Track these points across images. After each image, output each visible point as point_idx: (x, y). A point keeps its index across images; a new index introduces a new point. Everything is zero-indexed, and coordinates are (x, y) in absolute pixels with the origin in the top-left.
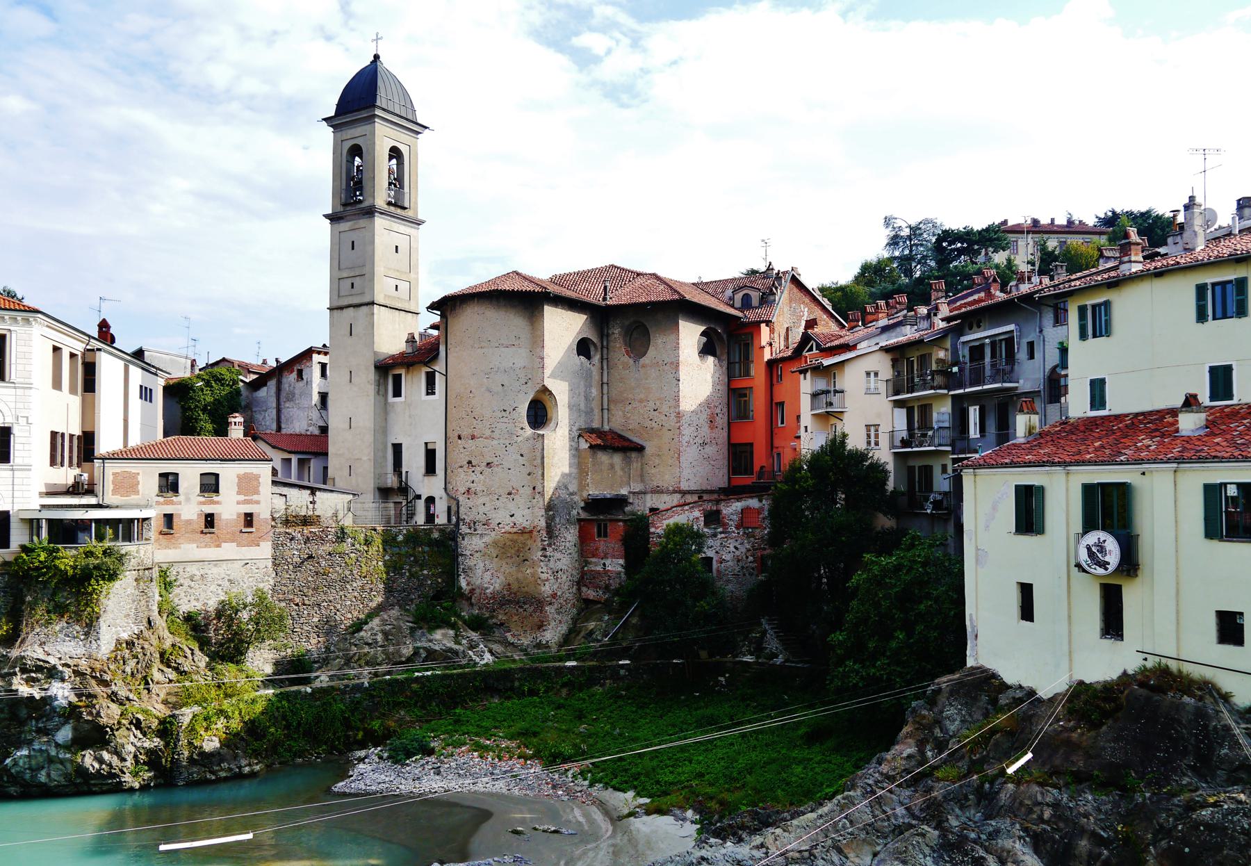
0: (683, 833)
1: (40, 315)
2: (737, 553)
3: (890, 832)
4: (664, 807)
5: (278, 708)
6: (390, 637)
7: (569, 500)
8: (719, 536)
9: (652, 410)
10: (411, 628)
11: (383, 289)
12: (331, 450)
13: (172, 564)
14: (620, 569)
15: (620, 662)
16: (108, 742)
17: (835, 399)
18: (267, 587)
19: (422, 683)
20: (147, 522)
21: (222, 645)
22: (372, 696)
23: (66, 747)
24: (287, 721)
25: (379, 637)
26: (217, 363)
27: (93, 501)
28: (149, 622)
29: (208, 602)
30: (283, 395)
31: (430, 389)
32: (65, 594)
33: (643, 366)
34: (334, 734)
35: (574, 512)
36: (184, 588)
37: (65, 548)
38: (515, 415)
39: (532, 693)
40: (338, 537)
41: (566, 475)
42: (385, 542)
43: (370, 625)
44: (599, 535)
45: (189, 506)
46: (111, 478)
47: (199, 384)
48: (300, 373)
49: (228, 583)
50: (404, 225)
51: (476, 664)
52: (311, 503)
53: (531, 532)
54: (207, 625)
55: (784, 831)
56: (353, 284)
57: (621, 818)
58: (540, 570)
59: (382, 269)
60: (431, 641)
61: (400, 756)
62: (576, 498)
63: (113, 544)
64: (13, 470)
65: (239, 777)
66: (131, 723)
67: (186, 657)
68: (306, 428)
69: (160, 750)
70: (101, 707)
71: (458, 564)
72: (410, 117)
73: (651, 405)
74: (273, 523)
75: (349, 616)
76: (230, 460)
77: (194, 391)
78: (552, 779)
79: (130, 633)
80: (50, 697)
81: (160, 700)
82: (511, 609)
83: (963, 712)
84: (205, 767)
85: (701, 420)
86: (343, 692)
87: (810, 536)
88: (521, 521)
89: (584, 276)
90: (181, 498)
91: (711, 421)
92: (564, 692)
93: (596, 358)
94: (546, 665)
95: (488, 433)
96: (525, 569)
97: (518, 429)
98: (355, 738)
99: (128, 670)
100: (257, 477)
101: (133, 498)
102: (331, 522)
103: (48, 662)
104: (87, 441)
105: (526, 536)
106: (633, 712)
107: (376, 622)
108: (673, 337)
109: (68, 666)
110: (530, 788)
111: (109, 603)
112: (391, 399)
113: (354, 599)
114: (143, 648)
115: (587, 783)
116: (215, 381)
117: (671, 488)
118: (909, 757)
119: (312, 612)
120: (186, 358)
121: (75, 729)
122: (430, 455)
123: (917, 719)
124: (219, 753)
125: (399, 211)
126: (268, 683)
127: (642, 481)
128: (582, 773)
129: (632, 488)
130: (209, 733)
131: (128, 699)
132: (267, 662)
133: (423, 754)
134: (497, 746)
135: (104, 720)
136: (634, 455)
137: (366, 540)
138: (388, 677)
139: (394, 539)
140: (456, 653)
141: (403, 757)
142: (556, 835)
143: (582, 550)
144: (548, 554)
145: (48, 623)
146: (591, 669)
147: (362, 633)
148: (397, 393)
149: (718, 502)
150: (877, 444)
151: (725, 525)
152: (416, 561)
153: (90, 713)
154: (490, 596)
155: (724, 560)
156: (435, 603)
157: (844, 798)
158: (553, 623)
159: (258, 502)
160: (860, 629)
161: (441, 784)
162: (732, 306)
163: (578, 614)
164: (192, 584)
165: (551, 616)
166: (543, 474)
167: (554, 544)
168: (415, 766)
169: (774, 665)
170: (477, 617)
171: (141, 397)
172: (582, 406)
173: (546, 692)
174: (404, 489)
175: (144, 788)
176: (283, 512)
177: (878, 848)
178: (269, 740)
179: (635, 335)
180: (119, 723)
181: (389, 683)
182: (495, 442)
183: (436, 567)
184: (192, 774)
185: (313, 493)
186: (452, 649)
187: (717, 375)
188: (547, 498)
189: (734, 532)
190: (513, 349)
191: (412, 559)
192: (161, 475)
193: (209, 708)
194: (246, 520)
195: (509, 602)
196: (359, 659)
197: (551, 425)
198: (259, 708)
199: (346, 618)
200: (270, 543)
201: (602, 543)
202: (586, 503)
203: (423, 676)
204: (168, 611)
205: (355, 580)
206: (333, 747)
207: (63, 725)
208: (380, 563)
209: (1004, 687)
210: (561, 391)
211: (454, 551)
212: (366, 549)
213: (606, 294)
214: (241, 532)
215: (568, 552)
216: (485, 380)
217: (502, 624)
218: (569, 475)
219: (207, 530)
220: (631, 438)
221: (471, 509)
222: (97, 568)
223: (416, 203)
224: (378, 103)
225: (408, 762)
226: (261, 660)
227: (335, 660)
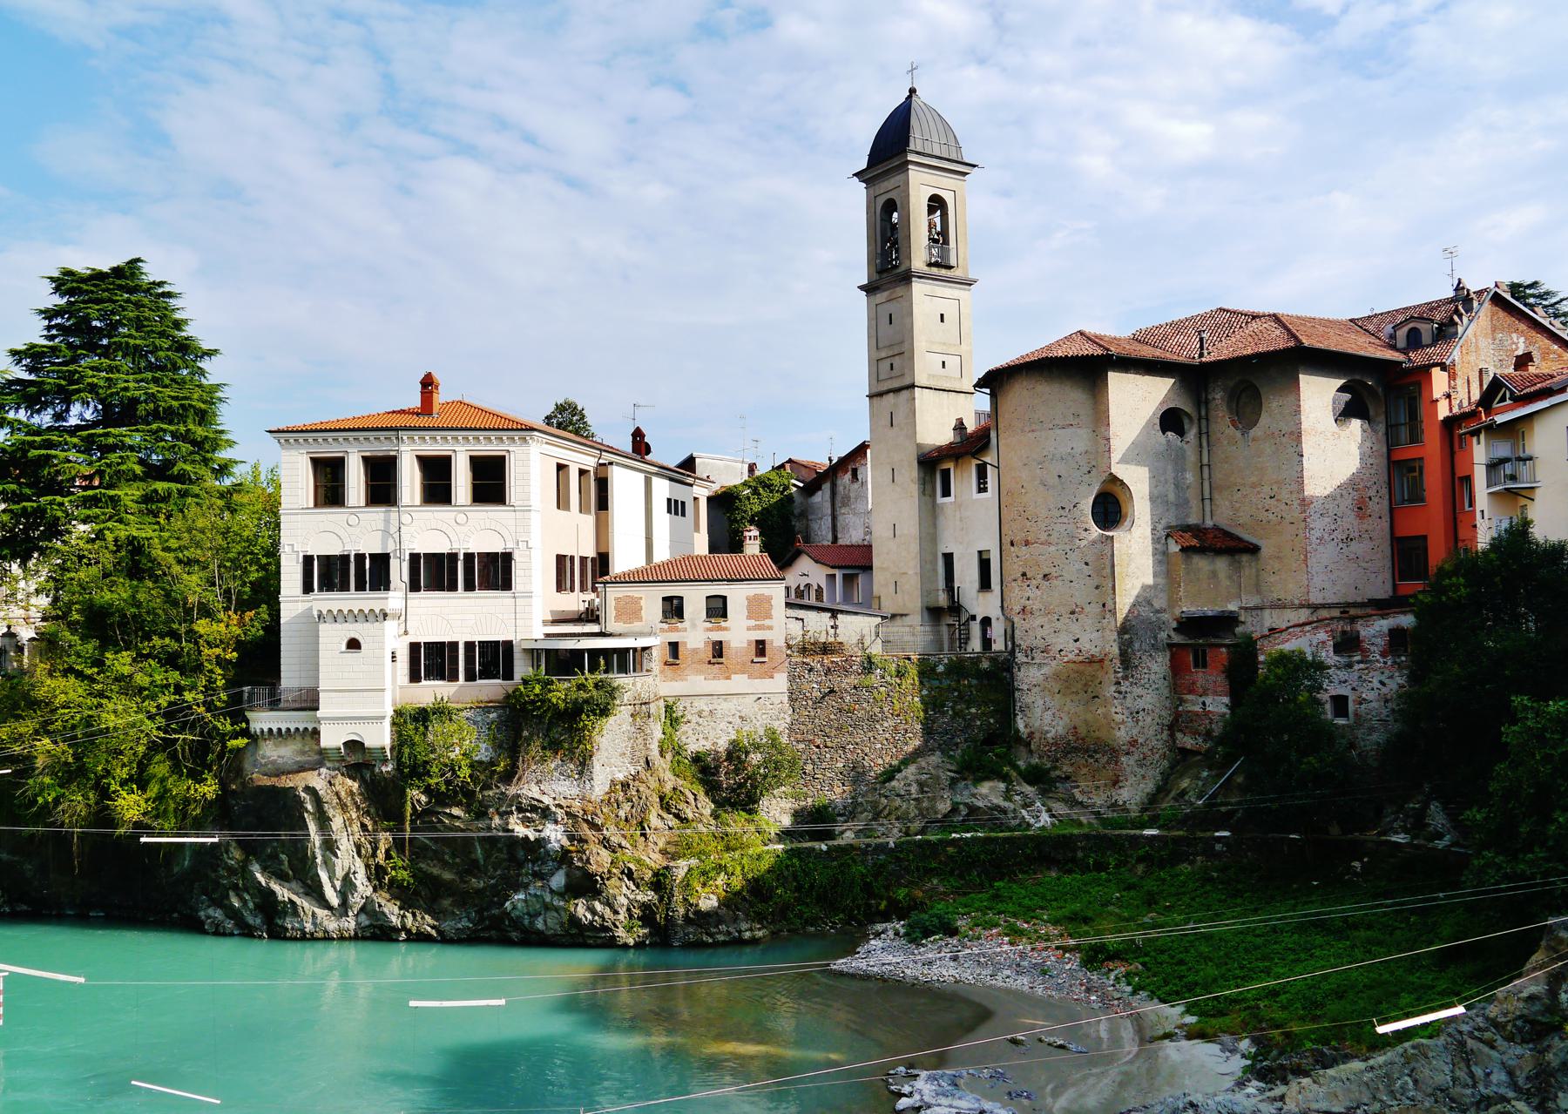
0: (1224, 1069)
1: (536, 433)
2: (1384, 690)
3: (1473, 1104)
4: (1210, 1031)
5: (787, 866)
6: (925, 789)
8: (1356, 667)
9: (1268, 497)
10: (952, 778)
11: (925, 368)
12: (876, 563)
13: (678, 697)
14: (1225, 710)
15: (1217, 834)
16: (599, 892)
17: (1524, 470)
18: (781, 726)
19: (960, 847)
20: (647, 651)
21: (733, 790)
22: (898, 859)
23: (561, 895)
24: (798, 882)
25: (914, 789)
27: (595, 628)
28: (647, 762)
29: (718, 741)
30: (839, 498)
32: (560, 729)
33: (1254, 440)
34: (853, 901)
35: (1163, 635)
36: (693, 725)
37: (559, 680)
38: (1076, 512)
39: (1100, 867)
40: (864, 668)
41: (1149, 586)
42: (921, 674)
43: (904, 773)
44: (1196, 666)
45: (695, 632)
46: (613, 603)
47: (745, 492)
48: (855, 473)
49: (739, 721)
50: (950, 287)
51: (1029, 825)
52: (832, 627)
53: (1101, 661)
54: (717, 768)
55: (1315, 1082)
56: (892, 365)
57: (1153, 1040)
58: (1113, 710)
59: (924, 344)
60: (974, 795)
61: (917, 935)
62: (1165, 617)
63: (606, 676)
64: (514, 597)
65: (738, 942)
66: (623, 873)
67: (687, 802)
68: (862, 537)
69: (654, 904)
70: (591, 853)
71: (1014, 701)
72: (960, 160)
73: (1266, 489)
74: (789, 652)
75: (880, 761)
76: (737, 580)
77: (740, 500)
78: (1090, 980)
79: (626, 774)
80: (544, 839)
81: (657, 850)
82: (1080, 760)
84: (701, 928)
85: (1342, 508)
86: (865, 852)
87: (1457, 669)
88: (1088, 646)
89: (1178, 327)
90: (686, 624)
91: (1360, 508)
92: (1140, 868)
93: (1192, 434)
94: (1117, 832)
95: (1043, 537)
96: (1095, 708)
97: (1080, 531)
98: (877, 907)
99: (622, 814)
100: (769, 599)
101: (636, 626)
102: (856, 649)
103: (541, 802)
104: (602, 562)
105: (1096, 666)
106: (1220, 901)
107: (912, 769)
108: (1291, 398)
109: (561, 807)
110: (1059, 988)
111: (604, 739)
112: (940, 500)
113: (885, 742)
114: (638, 791)
115: (1129, 989)
116: (763, 488)
117: (1297, 602)
118: (1532, 998)
119: (836, 756)
120: (743, 462)
121: (568, 875)
122: (984, 565)
123: (1553, 944)
124: (716, 913)
125: (943, 272)
126: (785, 835)
127: (1258, 592)
128: (1127, 975)
129: (1244, 601)
130: (706, 890)
131: (620, 846)
132: (783, 811)
133: (945, 934)
134: (1036, 931)
135: (593, 868)
136: (1245, 558)
137: (899, 672)
139: (933, 669)
140: (1004, 811)
141: (920, 936)
142: (1061, 1051)
143: (1175, 684)
144: (1123, 689)
145: (543, 760)
146: (1176, 840)
147: (894, 783)
148: (946, 493)
149: (1353, 619)
151: (1364, 651)
152: (961, 697)
153: (580, 859)
154: (1051, 741)
155: (1364, 699)
156: (987, 748)
157: (1413, 1047)
158: (1132, 779)
159: (770, 628)
160: (1510, 806)
161: (952, 972)
162: (1393, 347)
163: (1172, 768)
164: (701, 721)
165: (1128, 769)
166: (1114, 586)
167: (1132, 676)
168: (929, 950)
169: (1435, 849)
170: (1036, 767)
171: (669, 511)
172: (1172, 497)
173: (1117, 866)
174: (955, 608)
175: (639, 946)
176: (800, 638)
178: (776, 903)
180: (609, 872)
181: (920, 844)
182: (1052, 548)
183: (986, 705)
184: (687, 934)
186: (999, 807)
187: (1368, 444)
188: (1120, 617)
189: (1377, 661)
190: (1069, 431)
191: (956, 694)
192: (664, 599)
193: (707, 862)
194: (757, 648)
195: (1076, 750)
196: (889, 814)
197: (1126, 524)
198: (765, 865)
199: (877, 763)
200: (786, 674)
201: (1201, 675)
202: (1178, 622)
203: (961, 839)
204: (671, 747)
205: (885, 719)
206: (852, 917)
207: (557, 870)
208: (916, 699)
210: (1138, 481)
211: (1009, 684)
212: (899, 682)
213: (1202, 347)
214: (752, 662)
216: (1038, 471)
217: (1067, 778)
218: (1155, 587)
219: (713, 660)
221: (1032, 632)
222: (586, 701)
224: (912, 147)
225: (924, 941)
226: (777, 811)
227: (862, 813)
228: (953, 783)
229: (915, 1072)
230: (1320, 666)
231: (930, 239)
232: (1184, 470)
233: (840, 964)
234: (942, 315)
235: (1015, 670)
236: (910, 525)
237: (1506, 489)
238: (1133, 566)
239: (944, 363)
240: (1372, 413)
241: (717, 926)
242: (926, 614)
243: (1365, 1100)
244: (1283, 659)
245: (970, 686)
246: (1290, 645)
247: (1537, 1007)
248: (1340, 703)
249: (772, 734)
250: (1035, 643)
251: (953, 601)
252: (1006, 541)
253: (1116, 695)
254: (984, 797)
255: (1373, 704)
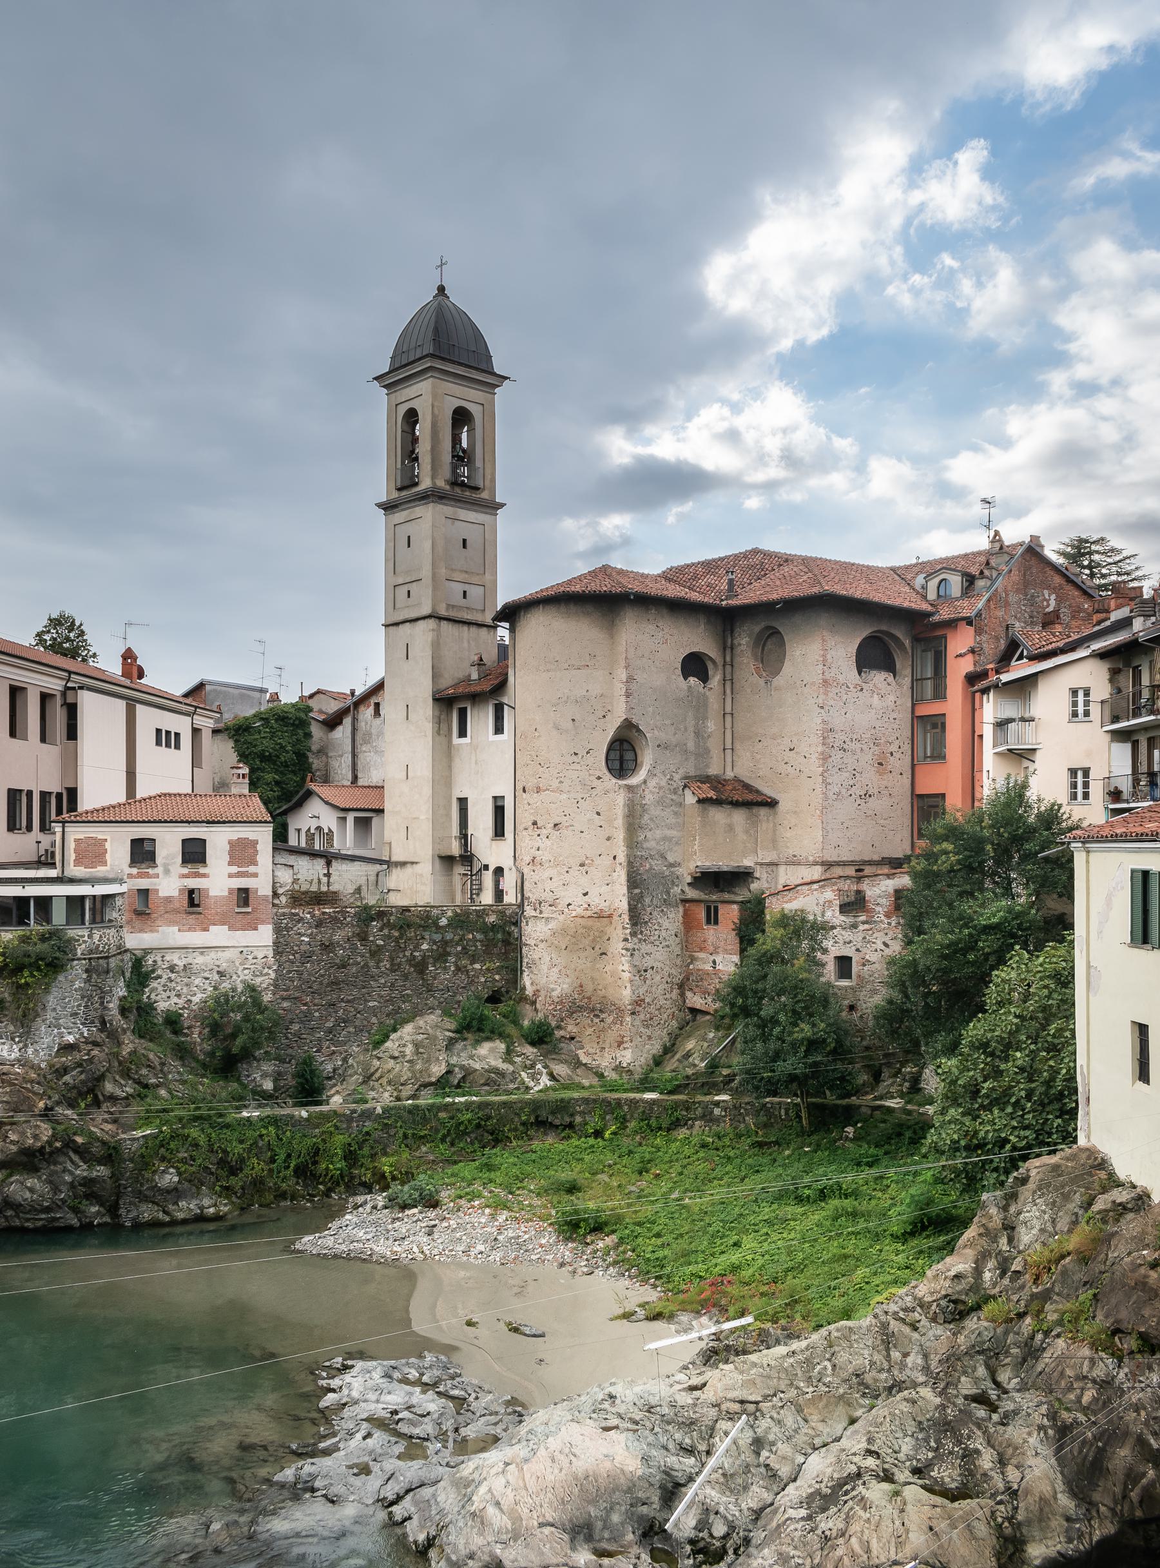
2: (888, 952)
6: (421, 1050)
7: (667, 873)
8: (861, 927)
10: (451, 1039)
13: (147, 952)
25: (409, 1050)
26: (311, 696)
27: (53, 873)
29: (193, 999)
31: (499, 729)
35: (676, 890)
36: (163, 981)
44: (708, 922)
48: (377, 705)
49: (216, 977)
53: (610, 916)
59: (444, 570)
72: (483, 366)
73: (786, 741)
82: (585, 1019)
83: (1046, 1217)
86: (349, 1119)
88: (597, 901)
89: (710, 566)
90: (159, 870)
94: (617, 1095)
95: (555, 784)
112: (456, 741)
118: (958, 1277)
122: (499, 811)
136: (763, 812)
138: (410, 1102)
146: (676, 1106)
148: (463, 733)
150: (1086, 796)
154: (557, 1000)
159: (255, 875)
164: (173, 976)
167: (641, 933)
174: (467, 858)
177: (859, 1413)
179: (769, 645)
181: (412, 1111)
182: (564, 796)
185: (329, 864)
200: (270, 927)
201: (712, 932)
209: (1113, 1182)
215: (664, 944)
220: (760, 788)
223: (493, 480)
227: (351, 1076)
228: (450, 1044)
229: (350, 1363)
230: (827, 927)
231: (453, 457)
232: (705, 718)
233: (307, 1242)
234: (464, 541)
235: (524, 924)
236: (423, 768)
237: (1009, 750)
238: (646, 817)
239: (465, 592)
240: (898, 666)
241: (176, 1203)
242: (437, 860)
243: (783, 1388)
244: (784, 921)
245: (474, 939)
246: (792, 905)
247: (963, 1285)
248: (844, 964)
249: (251, 989)
250: (544, 896)
251: (466, 851)
252: (519, 787)
253: (624, 952)
254: (482, 1059)
255: (876, 966)
